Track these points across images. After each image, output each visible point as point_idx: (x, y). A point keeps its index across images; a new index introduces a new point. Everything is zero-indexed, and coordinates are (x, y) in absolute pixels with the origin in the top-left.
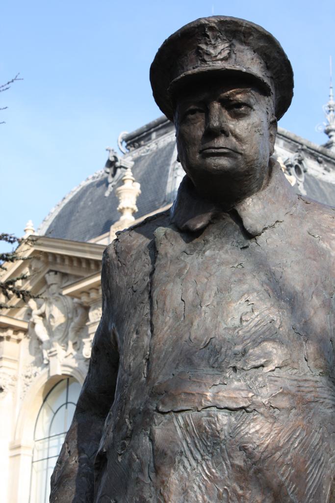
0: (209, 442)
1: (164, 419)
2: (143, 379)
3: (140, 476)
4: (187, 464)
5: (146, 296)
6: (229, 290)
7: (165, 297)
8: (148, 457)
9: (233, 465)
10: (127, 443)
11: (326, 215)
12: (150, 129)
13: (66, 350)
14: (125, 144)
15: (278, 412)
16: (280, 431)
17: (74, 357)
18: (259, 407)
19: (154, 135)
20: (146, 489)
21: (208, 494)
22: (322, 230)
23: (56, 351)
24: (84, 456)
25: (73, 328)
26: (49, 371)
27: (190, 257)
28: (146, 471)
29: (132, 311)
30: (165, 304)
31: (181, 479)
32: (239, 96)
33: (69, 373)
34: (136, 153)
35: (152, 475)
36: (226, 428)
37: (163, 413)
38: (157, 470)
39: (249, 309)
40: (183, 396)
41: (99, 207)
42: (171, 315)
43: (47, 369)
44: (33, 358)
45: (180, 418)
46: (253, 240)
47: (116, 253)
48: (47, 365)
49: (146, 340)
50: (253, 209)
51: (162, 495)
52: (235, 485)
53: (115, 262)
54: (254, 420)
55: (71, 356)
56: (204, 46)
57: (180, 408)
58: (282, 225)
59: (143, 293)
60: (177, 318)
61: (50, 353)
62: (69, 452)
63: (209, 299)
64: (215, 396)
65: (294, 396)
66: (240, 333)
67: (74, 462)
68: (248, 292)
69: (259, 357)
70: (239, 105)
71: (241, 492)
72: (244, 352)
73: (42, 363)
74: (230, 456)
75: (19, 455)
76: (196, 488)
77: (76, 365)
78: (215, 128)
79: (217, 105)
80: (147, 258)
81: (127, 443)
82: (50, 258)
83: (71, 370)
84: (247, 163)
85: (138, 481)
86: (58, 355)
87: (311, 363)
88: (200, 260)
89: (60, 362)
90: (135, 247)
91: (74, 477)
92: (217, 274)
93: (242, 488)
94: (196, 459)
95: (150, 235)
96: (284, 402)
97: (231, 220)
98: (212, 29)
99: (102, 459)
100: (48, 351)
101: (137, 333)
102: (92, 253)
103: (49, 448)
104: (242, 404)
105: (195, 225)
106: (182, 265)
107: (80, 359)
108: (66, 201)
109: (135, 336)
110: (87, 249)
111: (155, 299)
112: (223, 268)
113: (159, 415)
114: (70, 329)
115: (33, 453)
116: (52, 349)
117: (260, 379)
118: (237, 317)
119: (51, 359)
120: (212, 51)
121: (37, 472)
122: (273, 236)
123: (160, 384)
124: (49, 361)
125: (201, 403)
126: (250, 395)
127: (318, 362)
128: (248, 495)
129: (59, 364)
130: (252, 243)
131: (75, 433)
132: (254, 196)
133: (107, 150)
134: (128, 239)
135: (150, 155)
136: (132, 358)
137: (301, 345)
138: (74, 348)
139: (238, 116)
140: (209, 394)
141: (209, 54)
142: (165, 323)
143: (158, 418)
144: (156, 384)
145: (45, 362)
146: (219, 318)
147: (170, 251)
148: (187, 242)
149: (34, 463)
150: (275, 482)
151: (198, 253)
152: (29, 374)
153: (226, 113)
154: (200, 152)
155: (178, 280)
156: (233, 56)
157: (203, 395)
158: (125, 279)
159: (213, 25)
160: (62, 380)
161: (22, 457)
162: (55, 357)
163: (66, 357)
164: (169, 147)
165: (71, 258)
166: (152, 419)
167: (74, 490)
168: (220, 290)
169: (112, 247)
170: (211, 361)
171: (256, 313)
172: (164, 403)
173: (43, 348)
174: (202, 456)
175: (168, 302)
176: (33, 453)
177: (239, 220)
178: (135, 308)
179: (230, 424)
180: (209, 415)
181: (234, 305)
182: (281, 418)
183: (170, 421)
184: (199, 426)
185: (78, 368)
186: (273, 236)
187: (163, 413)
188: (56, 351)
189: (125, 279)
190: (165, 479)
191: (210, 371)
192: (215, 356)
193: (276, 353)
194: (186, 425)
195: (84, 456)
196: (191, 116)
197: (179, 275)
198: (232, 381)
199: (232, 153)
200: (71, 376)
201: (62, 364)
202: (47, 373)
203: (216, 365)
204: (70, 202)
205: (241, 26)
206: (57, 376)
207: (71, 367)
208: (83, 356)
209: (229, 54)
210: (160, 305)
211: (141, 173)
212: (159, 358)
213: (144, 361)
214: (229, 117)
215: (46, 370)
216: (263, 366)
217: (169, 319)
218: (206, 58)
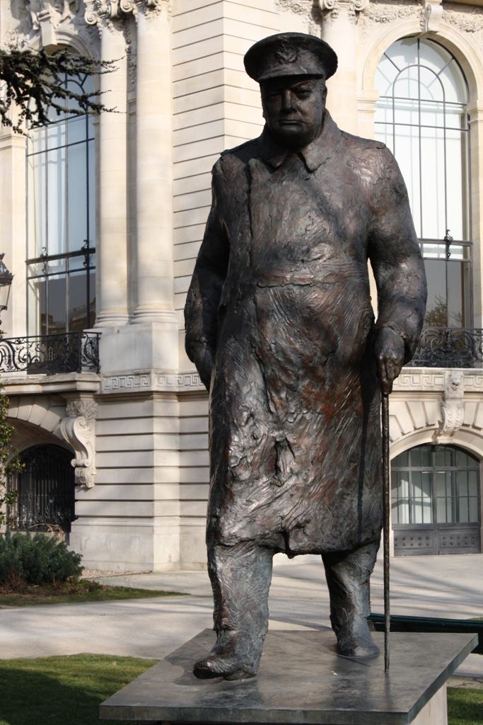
0: (290, 307)
1: (262, 291)
2: (248, 265)
3: (249, 323)
4: (276, 317)
5: (246, 208)
6: (298, 210)
7: (259, 212)
8: (253, 312)
9: (302, 317)
10: (240, 302)
11: (358, 149)
13: (61, 13)
15: (328, 285)
16: (329, 296)
17: (72, 22)
18: (317, 283)
20: (253, 330)
21: (288, 333)
22: (356, 161)
23: (48, 13)
24: (205, 299)
26: (41, 40)
27: (274, 185)
28: (252, 320)
29: (237, 216)
30: (259, 218)
31: (273, 325)
32: (303, 87)
33: (67, 43)
35: (256, 323)
36: (298, 296)
37: (261, 287)
38: (259, 320)
39: (310, 223)
40: (273, 278)
42: (263, 224)
43: (39, 37)
44: (18, 22)
45: (271, 291)
46: (312, 174)
47: (223, 170)
48: (38, 31)
49: (248, 239)
50: (312, 153)
51: (262, 334)
52: (303, 328)
53: (223, 177)
54: (314, 291)
55: (68, 21)
56: (280, 53)
57: (271, 285)
58: (331, 161)
59: (244, 206)
60: (267, 227)
61: (41, 16)
62: (195, 295)
63: (286, 216)
64: (292, 277)
65: (337, 275)
66: (306, 238)
67: (199, 303)
68: (310, 211)
69: (317, 253)
70: (303, 91)
71: (307, 332)
72: (308, 251)
73: (32, 28)
74: (301, 312)
75: (10, 147)
76: (281, 330)
77: (76, 33)
78: (289, 109)
79: (289, 92)
80: (244, 178)
81: (240, 302)
83: (70, 39)
84: (308, 128)
85: (247, 325)
86: (51, 20)
87: (348, 253)
88: (280, 188)
89: (55, 28)
90: (236, 168)
91: (200, 313)
92: (291, 198)
93: (307, 329)
94: (281, 314)
95: (245, 160)
96: (332, 280)
97: (298, 158)
98: (285, 42)
99: (223, 309)
100: (38, 14)
101: (241, 233)
103: (46, 138)
104: (308, 283)
105: (276, 164)
106: (268, 190)
107: (80, 25)
109: (240, 235)
111: (252, 212)
112: (294, 194)
113: (259, 289)
115: (27, 144)
116: (44, 12)
117: (318, 267)
118: (304, 228)
119: (42, 24)
120: (285, 57)
121: (33, 168)
122: (326, 170)
123: (259, 270)
124: (39, 26)
125: (283, 282)
126: (312, 276)
127: (352, 253)
128: (311, 333)
129: (53, 31)
130: (312, 176)
131: (197, 282)
132: (312, 144)
134: (230, 161)
136: (240, 249)
137: (342, 243)
138: (71, 10)
139: (303, 98)
140: (288, 276)
142: (259, 230)
143: (258, 290)
144: (256, 270)
145: (35, 28)
146: (293, 229)
147: (260, 180)
148: (271, 172)
149: (29, 157)
150: (326, 325)
151: (278, 183)
153: (295, 96)
154: (279, 121)
155: (267, 201)
156: (299, 58)
157: (285, 278)
158: (230, 190)
159: (286, 40)
161: (13, 149)
162: (47, 22)
163: (62, 21)
166: (255, 291)
167: (202, 322)
168: (292, 210)
169: (219, 164)
170: (289, 257)
171: (315, 225)
172: (262, 282)
173: (30, 9)
174: (285, 312)
175: (261, 216)
176: (27, 144)
177: (304, 160)
178: (239, 215)
179: (300, 294)
180: (289, 289)
181: (301, 220)
182: (330, 288)
183: (266, 292)
184: (283, 296)
185: (78, 36)
186: (326, 170)
187: (261, 287)
188: (48, 13)
189: (230, 190)
190: (263, 325)
191: (288, 263)
192: (294, 254)
193: (327, 249)
194: (275, 294)
195: (205, 299)
196: (273, 98)
197: (267, 197)
198: (301, 269)
199: (298, 123)
200: (70, 46)
201: (57, 30)
202: (38, 42)
203: (292, 259)
205: (304, 39)
206: (52, 46)
207: (69, 35)
208: (84, 20)
209: (296, 58)
210: (256, 217)
212: (257, 253)
213: (248, 253)
214: (297, 99)
215: (36, 38)
216: (319, 258)
217: (262, 227)
218: (282, 61)
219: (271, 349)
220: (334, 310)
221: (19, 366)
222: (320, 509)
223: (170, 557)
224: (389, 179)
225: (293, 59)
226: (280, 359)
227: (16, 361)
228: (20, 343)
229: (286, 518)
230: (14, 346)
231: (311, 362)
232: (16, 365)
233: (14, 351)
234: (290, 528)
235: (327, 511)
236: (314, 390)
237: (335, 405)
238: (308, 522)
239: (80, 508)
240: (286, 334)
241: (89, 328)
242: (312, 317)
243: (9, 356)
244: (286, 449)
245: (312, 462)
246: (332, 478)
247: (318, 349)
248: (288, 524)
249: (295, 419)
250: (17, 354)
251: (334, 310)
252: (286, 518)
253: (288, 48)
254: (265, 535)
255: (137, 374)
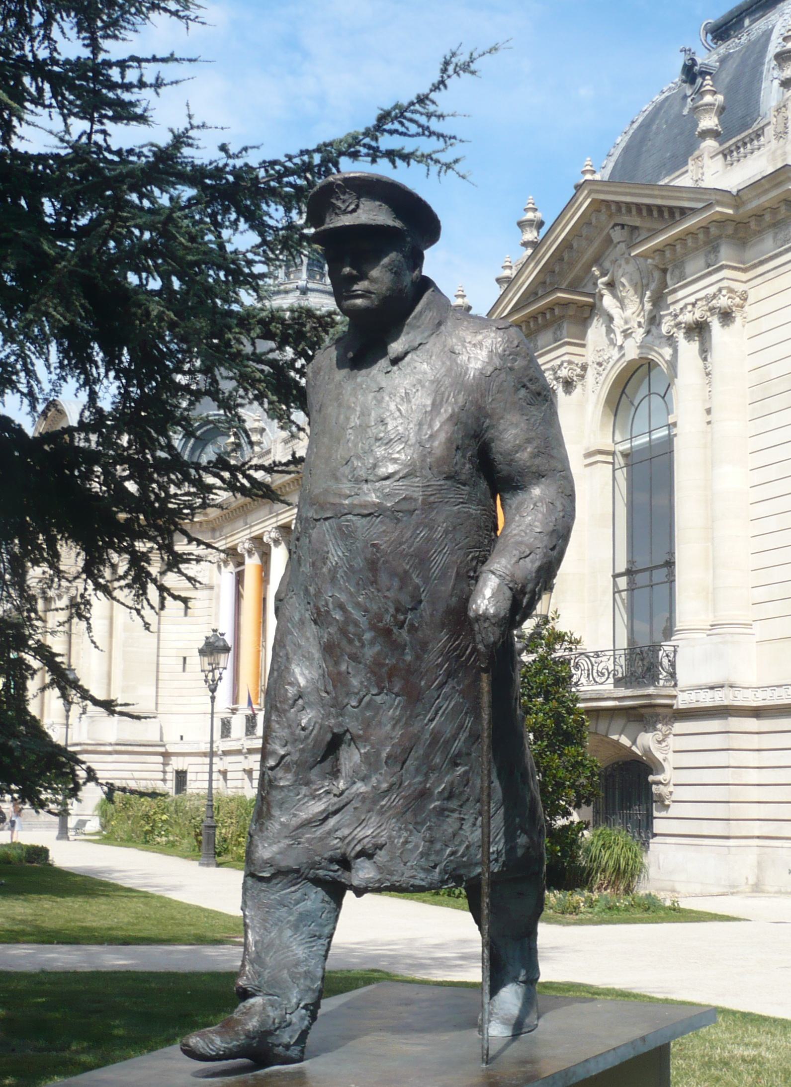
12: (741, 13)
14: (710, 37)
15: (401, 514)
19: (747, 22)
25: (649, 298)
34: (722, 49)
41: (676, 131)
82: (613, 207)
102: (663, 197)
104: (371, 511)
108: (635, 126)
110: (656, 192)
114: (646, 299)
133: (681, 51)
135: (740, 51)
141: (340, 208)
152: (601, 360)
160: (642, 366)
164: (764, 39)
165: (639, 206)
204: (640, 126)
211: (728, 79)
219: (327, 605)
220: (412, 549)
221: (597, 679)
222: (400, 829)
223: (747, 879)
224: (511, 369)
225: (352, 207)
226: (337, 618)
227: (595, 675)
228: (598, 656)
229: (347, 841)
230: (593, 660)
231: (381, 621)
232: (594, 679)
233: (592, 665)
234: (353, 854)
235: (411, 832)
236: (387, 662)
237: (423, 683)
238: (381, 847)
239: (659, 826)
240: (344, 582)
241: (666, 641)
242: (378, 559)
243: (588, 670)
244: (349, 745)
245: (386, 762)
246: (421, 786)
247: (391, 604)
248: (349, 850)
249: (360, 701)
250: (595, 668)
251: (412, 549)
252: (347, 841)
253: (344, 193)
254: (315, 863)
255: (712, 688)
